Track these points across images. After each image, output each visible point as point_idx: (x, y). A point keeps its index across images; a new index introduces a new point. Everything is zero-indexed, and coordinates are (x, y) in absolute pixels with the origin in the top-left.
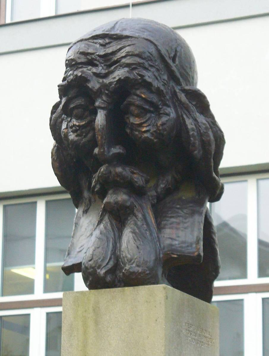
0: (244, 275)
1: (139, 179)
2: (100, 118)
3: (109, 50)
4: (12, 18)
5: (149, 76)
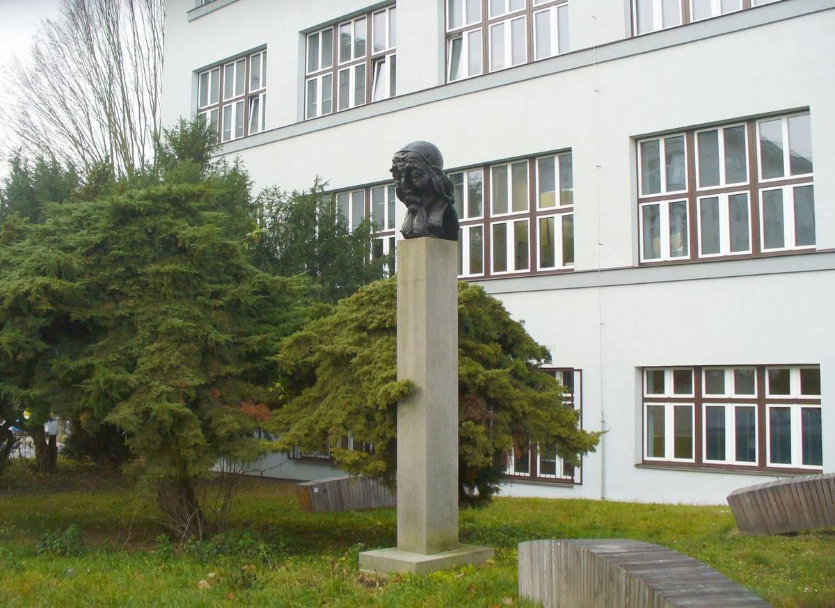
0: (782, 175)
1: (418, 200)
2: (403, 180)
3: (404, 156)
4: (537, 58)
5: (416, 165)
